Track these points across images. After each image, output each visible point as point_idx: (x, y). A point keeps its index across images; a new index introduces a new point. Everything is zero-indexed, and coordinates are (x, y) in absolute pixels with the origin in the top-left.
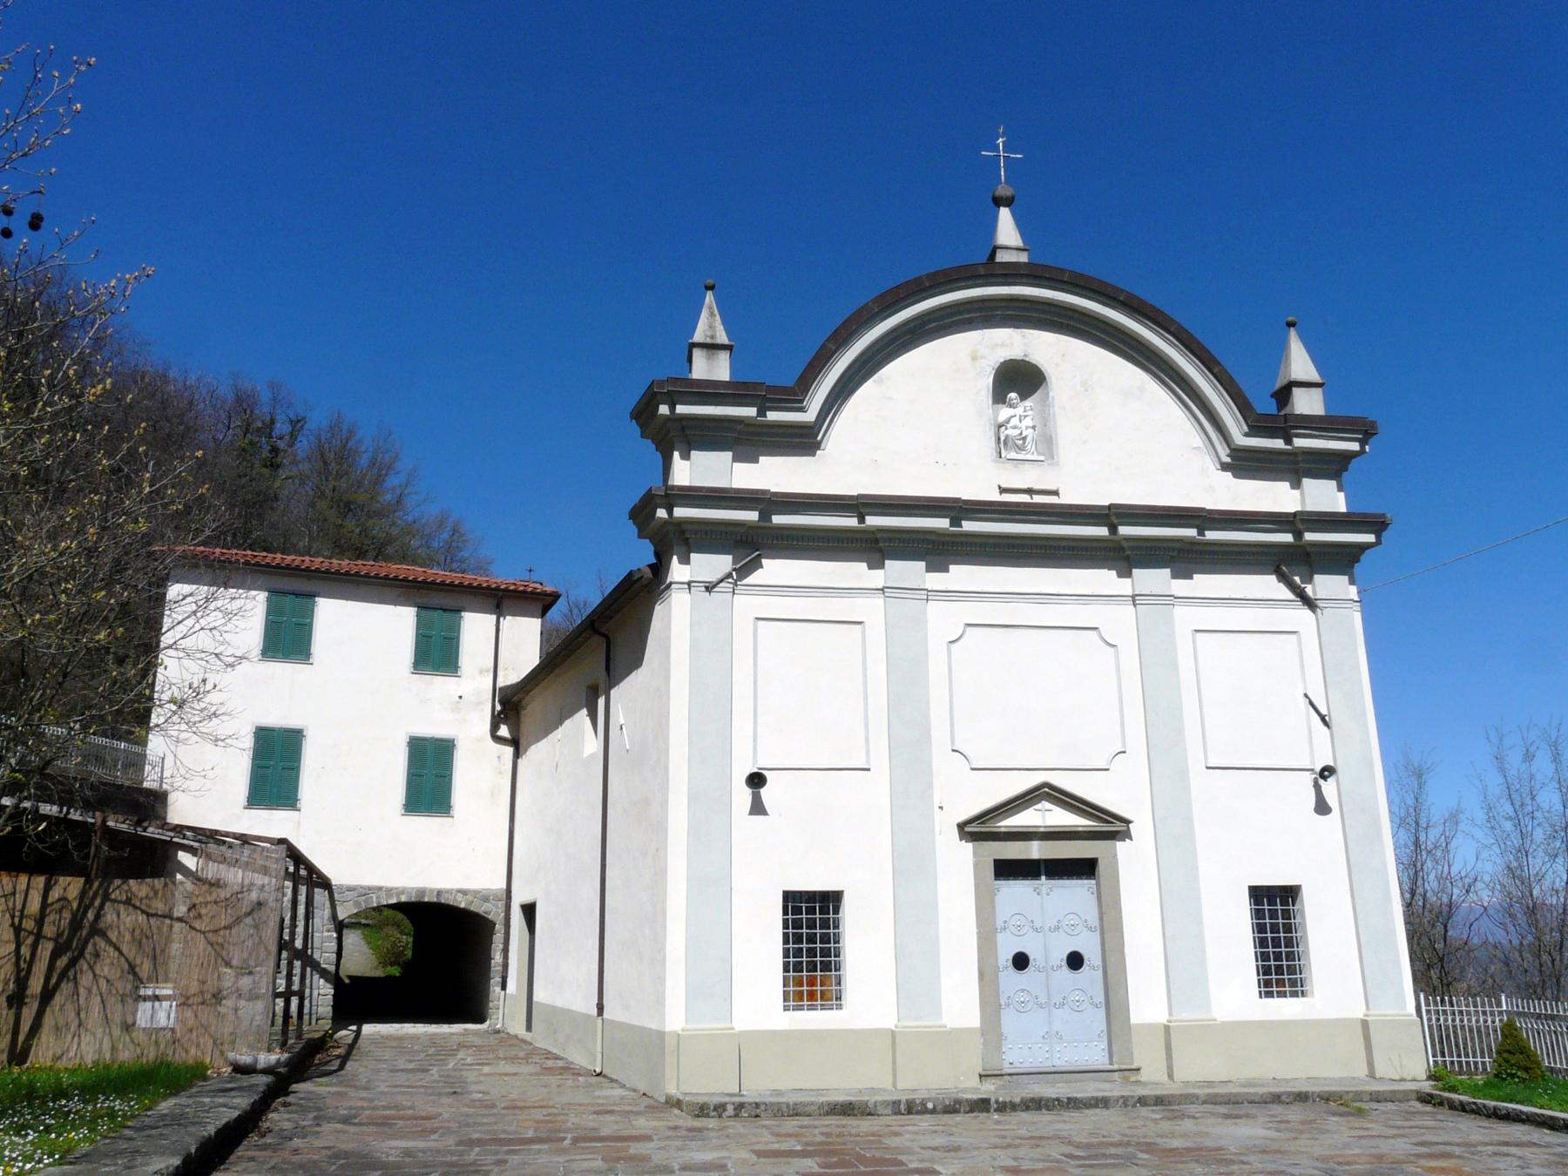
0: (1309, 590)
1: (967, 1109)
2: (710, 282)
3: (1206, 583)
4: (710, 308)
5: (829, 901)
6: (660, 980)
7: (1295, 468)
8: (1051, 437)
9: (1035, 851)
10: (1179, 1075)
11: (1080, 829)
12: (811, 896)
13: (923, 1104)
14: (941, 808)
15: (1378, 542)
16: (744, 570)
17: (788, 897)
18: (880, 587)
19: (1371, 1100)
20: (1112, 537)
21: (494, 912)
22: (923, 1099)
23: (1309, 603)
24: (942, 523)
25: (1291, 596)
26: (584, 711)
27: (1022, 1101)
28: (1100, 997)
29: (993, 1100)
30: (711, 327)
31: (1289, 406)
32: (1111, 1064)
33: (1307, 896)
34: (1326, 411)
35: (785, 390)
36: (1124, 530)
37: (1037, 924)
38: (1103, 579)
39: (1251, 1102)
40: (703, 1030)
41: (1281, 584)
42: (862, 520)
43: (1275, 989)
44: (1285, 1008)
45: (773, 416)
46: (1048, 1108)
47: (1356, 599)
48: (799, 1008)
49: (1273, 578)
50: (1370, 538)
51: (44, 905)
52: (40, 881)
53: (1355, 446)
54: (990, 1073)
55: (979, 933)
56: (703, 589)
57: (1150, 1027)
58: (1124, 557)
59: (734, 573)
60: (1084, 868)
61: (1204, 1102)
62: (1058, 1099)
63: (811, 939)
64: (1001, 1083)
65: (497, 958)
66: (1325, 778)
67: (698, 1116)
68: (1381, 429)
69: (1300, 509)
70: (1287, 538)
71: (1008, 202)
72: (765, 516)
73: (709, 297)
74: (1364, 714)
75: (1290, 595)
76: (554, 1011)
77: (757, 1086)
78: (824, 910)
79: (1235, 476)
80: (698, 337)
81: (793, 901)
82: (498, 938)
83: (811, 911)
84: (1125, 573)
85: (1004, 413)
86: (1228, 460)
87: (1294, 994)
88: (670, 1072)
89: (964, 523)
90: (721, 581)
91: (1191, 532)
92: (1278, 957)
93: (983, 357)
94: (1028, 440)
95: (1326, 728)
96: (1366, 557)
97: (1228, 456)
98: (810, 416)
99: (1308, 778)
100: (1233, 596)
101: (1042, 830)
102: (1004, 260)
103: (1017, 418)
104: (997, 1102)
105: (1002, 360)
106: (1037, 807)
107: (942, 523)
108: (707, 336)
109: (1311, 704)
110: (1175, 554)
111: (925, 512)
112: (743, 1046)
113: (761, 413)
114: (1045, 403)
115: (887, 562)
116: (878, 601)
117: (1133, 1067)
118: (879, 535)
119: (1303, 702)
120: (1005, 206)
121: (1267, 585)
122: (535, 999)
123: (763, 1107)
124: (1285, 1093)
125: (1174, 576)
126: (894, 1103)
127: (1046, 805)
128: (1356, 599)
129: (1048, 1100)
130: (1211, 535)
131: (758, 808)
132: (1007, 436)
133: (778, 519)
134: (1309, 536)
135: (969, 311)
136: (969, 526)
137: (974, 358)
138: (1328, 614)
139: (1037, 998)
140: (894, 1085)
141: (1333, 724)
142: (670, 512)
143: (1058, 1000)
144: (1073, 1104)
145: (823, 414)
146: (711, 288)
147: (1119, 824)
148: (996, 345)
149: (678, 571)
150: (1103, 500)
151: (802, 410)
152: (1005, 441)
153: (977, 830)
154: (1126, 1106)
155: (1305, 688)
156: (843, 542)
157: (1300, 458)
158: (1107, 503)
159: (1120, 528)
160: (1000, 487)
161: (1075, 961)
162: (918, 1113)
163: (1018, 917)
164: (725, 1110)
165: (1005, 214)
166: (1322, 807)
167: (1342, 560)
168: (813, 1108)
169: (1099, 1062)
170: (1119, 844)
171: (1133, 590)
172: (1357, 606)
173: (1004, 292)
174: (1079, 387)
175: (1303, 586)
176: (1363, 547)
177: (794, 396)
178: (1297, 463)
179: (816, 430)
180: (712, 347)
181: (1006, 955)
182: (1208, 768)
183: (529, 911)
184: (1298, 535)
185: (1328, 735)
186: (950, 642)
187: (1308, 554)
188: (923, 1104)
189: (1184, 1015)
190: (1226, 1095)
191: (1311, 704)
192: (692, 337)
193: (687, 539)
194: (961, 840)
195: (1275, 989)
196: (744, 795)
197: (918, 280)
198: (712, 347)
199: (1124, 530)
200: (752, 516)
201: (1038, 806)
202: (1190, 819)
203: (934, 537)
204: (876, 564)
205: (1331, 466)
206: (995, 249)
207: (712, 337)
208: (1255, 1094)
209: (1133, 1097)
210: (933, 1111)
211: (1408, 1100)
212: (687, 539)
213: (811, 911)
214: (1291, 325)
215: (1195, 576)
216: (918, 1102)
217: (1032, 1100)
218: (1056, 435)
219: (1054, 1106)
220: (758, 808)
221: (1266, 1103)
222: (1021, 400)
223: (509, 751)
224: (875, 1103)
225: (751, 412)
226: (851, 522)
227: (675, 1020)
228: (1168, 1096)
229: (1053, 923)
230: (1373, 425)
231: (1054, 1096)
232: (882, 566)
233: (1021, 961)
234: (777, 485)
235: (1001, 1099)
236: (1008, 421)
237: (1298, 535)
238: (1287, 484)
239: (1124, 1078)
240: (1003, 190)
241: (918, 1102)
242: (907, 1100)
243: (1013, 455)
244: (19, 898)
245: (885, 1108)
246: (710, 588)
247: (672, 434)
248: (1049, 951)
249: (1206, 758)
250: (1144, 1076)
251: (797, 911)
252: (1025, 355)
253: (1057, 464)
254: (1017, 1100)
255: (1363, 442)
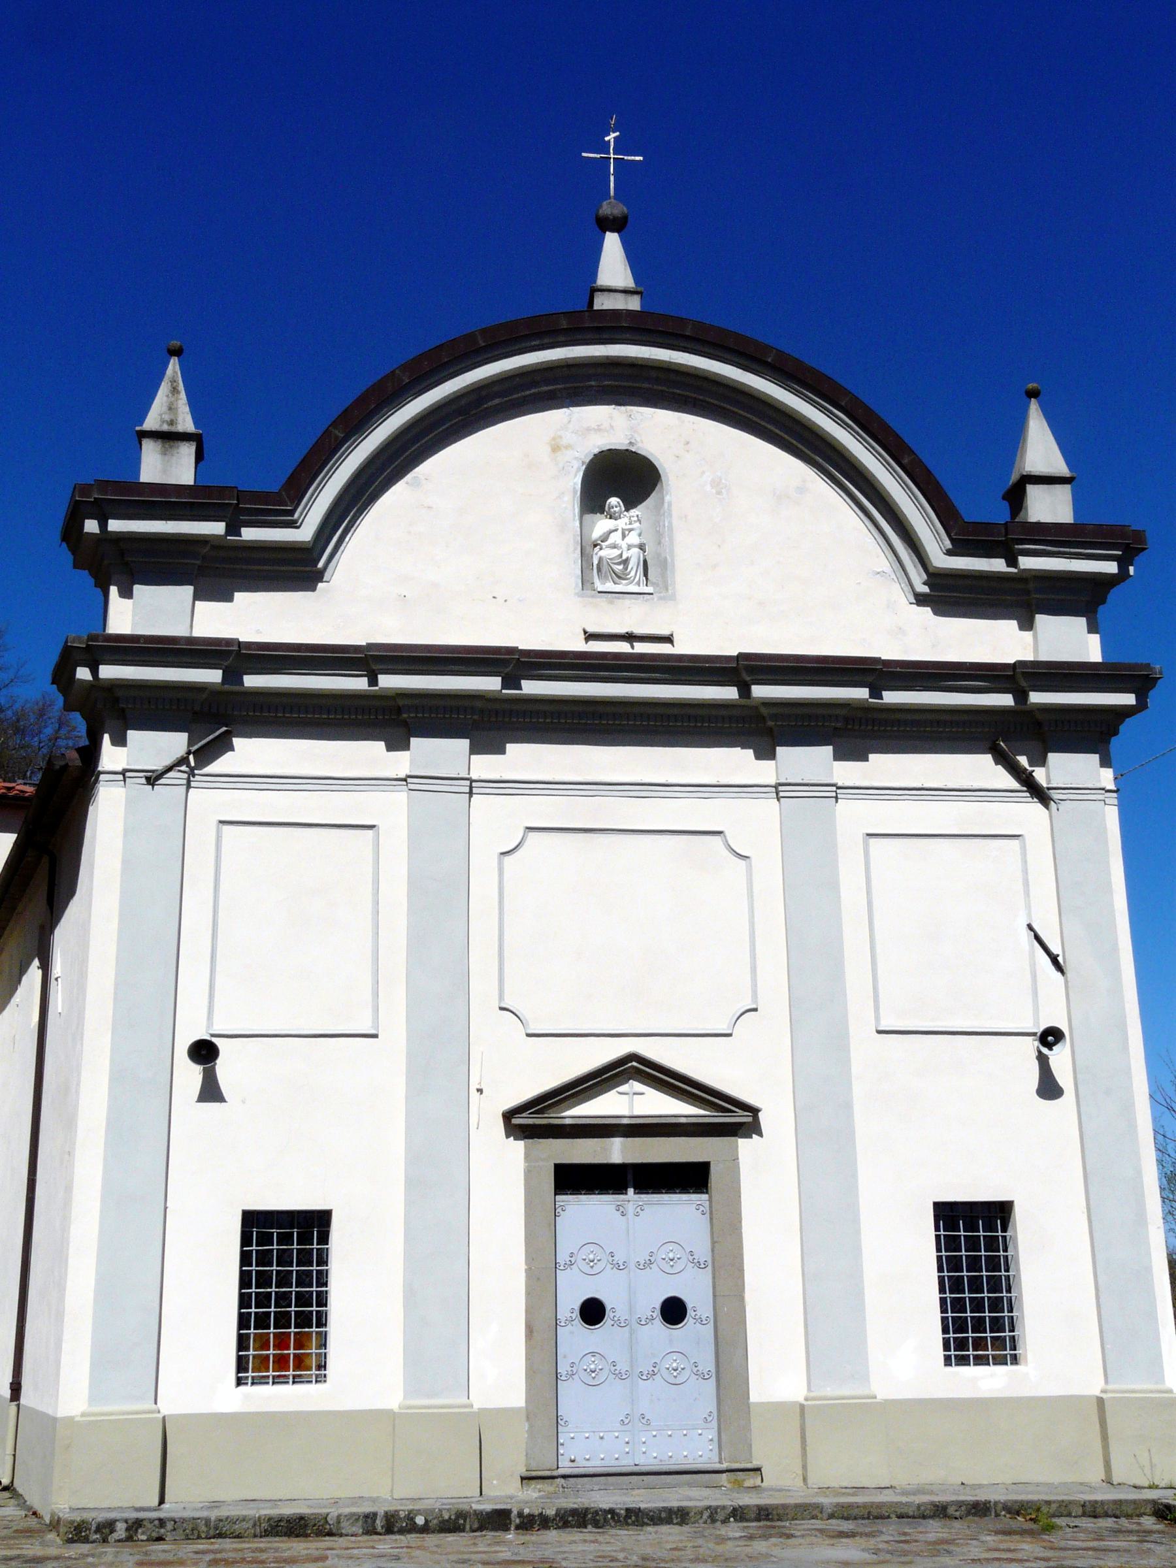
0: (1040, 775)
1: (476, 1526)
2: (175, 343)
4: (173, 381)
8: (666, 559)
9: (617, 1151)
10: (815, 1479)
11: (683, 1120)
13: (410, 1517)
14: (480, 1091)
15: (1141, 705)
16: (206, 753)
18: (402, 775)
19: (1084, 1515)
20: (744, 702)
22: (410, 1512)
23: (1040, 794)
24: (491, 684)
25: (1014, 784)
26: (36, 963)
27: (557, 1514)
29: (515, 1512)
30: (171, 408)
31: (1022, 514)
32: (720, 1462)
33: (1020, 1215)
34: (1074, 520)
35: (265, 497)
36: (760, 691)
37: (619, 1258)
39: (901, 1516)
40: (112, 1414)
41: (1000, 767)
42: (373, 681)
43: (971, 1352)
45: (249, 534)
46: (596, 1525)
47: (1112, 787)
48: (262, 1381)
49: (988, 758)
50: (1129, 699)
53: (1111, 567)
54: (534, 1474)
55: (529, 1272)
56: (143, 781)
57: (779, 1409)
59: (191, 757)
61: (832, 1516)
62: (612, 1511)
63: (284, 1279)
64: (551, 1489)
66: (1050, 1046)
67: (71, 1541)
68: (1151, 540)
69: (1030, 657)
70: (1006, 700)
71: (617, 225)
72: (233, 676)
73: (173, 367)
74: (1115, 949)
75: (1012, 783)
78: (305, 1239)
79: (936, 613)
80: (152, 422)
83: (285, 1239)
84: (766, 753)
85: (601, 525)
86: (925, 589)
87: (1000, 1361)
89: (524, 683)
90: (169, 769)
91: (862, 693)
92: (978, 1305)
93: (568, 447)
94: (632, 564)
95: (1059, 973)
96: (1127, 727)
97: (924, 583)
98: (305, 533)
99: (1031, 1046)
100: (926, 786)
101: (625, 1121)
102: (605, 307)
103: (619, 532)
104: (520, 1515)
105: (596, 451)
106: (622, 1088)
107: (491, 684)
108: (163, 422)
109: (1037, 938)
110: (839, 725)
111: (463, 668)
113: (233, 529)
115: (414, 741)
116: (400, 797)
117: (749, 1466)
118: (401, 702)
119: (1027, 936)
120: (612, 231)
123: (170, 1526)
124: (953, 1503)
125: (838, 756)
126: (366, 1516)
127: (636, 1086)
128: (1112, 787)
129: (596, 1513)
130: (891, 697)
131: (211, 1092)
132: (601, 559)
133: (252, 681)
135: (547, 382)
136: (531, 687)
137: (556, 448)
138: (1067, 809)
139: (614, 1364)
140: (392, 1496)
141: (1068, 969)
142: (95, 672)
143: (646, 1368)
144: (635, 1518)
145: (327, 531)
146: (177, 352)
147: (741, 1112)
148: (588, 429)
149: (111, 757)
150: (730, 648)
151: (293, 525)
152: (598, 565)
154: (714, 1521)
155: (1029, 915)
156: (276, 711)
157: (1031, 586)
158: (734, 652)
159: (1031, 694)
160: (585, 632)
161: (673, 1311)
162: (402, 1531)
163: (592, 1247)
164: (112, 1531)
165: (612, 243)
166: (1049, 1088)
168: (245, 1525)
169: (703, 1459)
170: (742, 1143)
171: (778, 779)
172: (1113, 799)
173: (597, 354)
174: (708, 488)
175: (1030, 769)
176: (1120, 714)
178: (1028, 592)
179: (315, 555)
180: (169, 438)
181: (570, 1302)
182: (879, 1032)
184: (1021, 696)
185: (1063, 981)
186: (502, 854)
187: (1039, 724)
188: (410, 1517)
189: (1135, 1384)
190: (865, 1505)
191: (1037, 938)
192: (141, 424)
193: (123, 710)
194: (507, 1137)
195: (971, 1352)
196: (191, 1075)
197: (470, 338)
198: (169, 438)
199: (760, 691)
200: (213, 676)
201: (624, 1088)
202: (848, 1106)
203: (479, 704)
204: (397, 743)
206: (594, 291)
207: (172, 423)
208: (907, 1504)
209: (724, 1508)
210: (425, 1529)
211: (1140, 1515)
212: (123, 710)
213: (285, 1239)
214: (1033, 394)
215: (871, 756)
216: (402, 1514)
217: (574, 1512)
218: (672, 556)
219: (605, 1519)
220: (211, 1092)
221: (924, 1517)
222: (627, 510)
224: (339, 1516)
225: (217, 528)
226: (358, 684)
228: (776, 1507)
229: (643, 1258)
230: (1139, 536)
231: (606, 1506)
232: (406, 747)
233: (593, 1312)
234: (258, 632)
235: (526, 1511)
236: (605, 538)
237: (1021, 696)
238: (1014, 624)
239: (736, 1482)
240: (610, 208)
241: (402, 1514)
242: (386, 1513)
243: (610, 586)
245: (352, 1524)
246: (153, 779)
247: (106, 562)
249: (877, 1018)
250: (771, 1478)
251: (265, 1239)
252: (631, 443)
253: (673, 598)
254: (551, 1512)
255: (1123, 563)
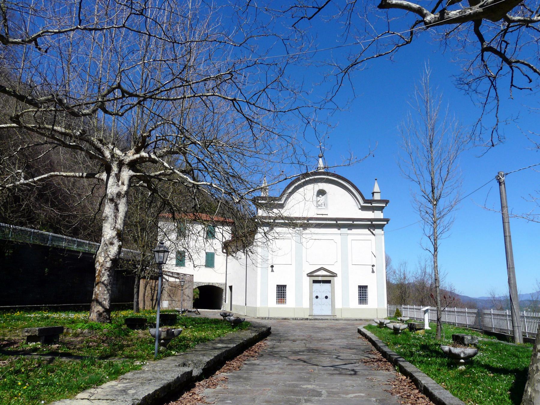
3: (354, 231)
5: (285, 286)
6: (256, 299)
7: (373, 209)
9: (320, 279)
12: (281, 286)
17: (277, 286)
21: (223, 288)
28: (330, 303)
36: (338, 222)
38: (335, 230)
44: (363, 306)
50: (386, 223)
51: (155, 285)
52: (154, 281)
53: (384, 205)
58: (339, 227)
60: (329, 282)
65: (224, 296)
75: (371, 233)
76: (237, 306)
77: (271, 316)
78: (284, 288)
81: (360, 287)
82: (224, 292)
83: (281, 288)
85: (319, 199)
88: (258, 313)
91: (351, 222)
98: (282, 202)
112: (269, 310)
114: (326, 196)
121: (366, 231)
122: (233, 304)
127: (322, 271)
131: (272, 271)
134: (373, 223)
153: (310, 275)
161: (326, 297)
166: (373, 272)
167: (381, 227)
177: (280, 199)
181: (314, 296)
183: (231, 287)
184: (372, 222)
199: (338, 222)
205: (381, 209)
213: (281, 288)
214: (376, 180)
220: (272, 271)
223: (226, 255)
227: (258, 305)
233: (317, 297)
237: (372, 222)
244: (151, 284)
248: (322, 296)
251: (279, 288)
